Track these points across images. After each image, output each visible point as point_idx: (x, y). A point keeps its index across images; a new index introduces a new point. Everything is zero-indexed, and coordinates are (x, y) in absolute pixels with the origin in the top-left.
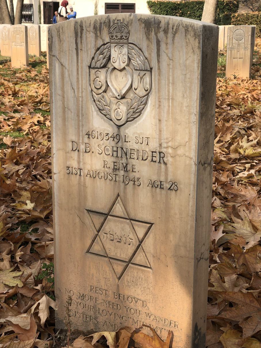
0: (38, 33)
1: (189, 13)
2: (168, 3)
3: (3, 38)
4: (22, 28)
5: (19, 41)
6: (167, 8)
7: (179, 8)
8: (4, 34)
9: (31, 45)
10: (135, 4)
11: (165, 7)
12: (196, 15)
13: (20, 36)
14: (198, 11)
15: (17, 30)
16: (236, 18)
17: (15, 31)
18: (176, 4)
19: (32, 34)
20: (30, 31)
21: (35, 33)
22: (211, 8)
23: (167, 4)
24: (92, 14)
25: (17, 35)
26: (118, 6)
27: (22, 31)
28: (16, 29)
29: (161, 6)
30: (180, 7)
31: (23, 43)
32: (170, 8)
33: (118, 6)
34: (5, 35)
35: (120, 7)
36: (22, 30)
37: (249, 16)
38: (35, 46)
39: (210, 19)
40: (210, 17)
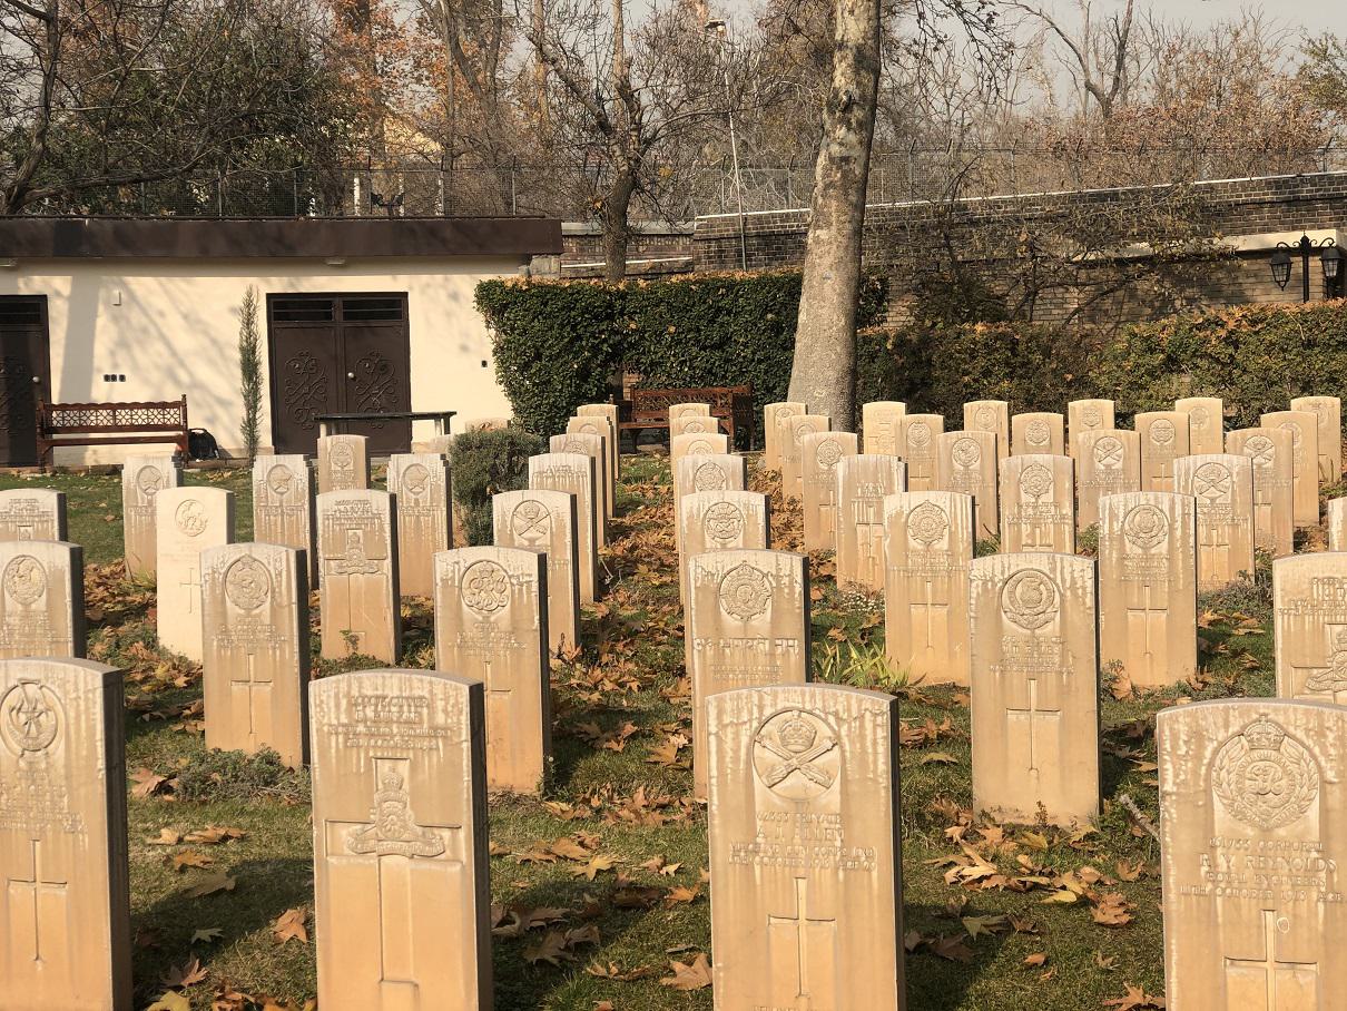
0: (295, 607)
1: (672, 329)
2: (578, 292)
3: (11, 634)
4: (440, 704)
5: (409, 811)
6: (573, 313)
7: (623, 308)
8: (20, 607)
9: (236, 688)
10: (405, 294)
11: (563, 308)
12: (706, 339)
13: (414, 769)
14: (712, 321)
15: (389, 722)
16: (914, 353)
17: (361, 728)
18: (609, 293)
19: (248, 610)
20: (230, 587)
21: (268, 604)
22: (835, 318)
23: (572, 294)
24: (416, 408)
25: (385, 766)
26: (329, 305)
27: (434, 728)
28: (370, 713)
29: (546, 304)
30: (630, 307)
31: (446, 834)
32: (585, 310)
33: (329, 305)
34: (27, 615)
35: (338, 314)
36: (440, 719)
37: (975, 343)
38: (268, 688)
39: (838, 367)
40: (834, 357)
